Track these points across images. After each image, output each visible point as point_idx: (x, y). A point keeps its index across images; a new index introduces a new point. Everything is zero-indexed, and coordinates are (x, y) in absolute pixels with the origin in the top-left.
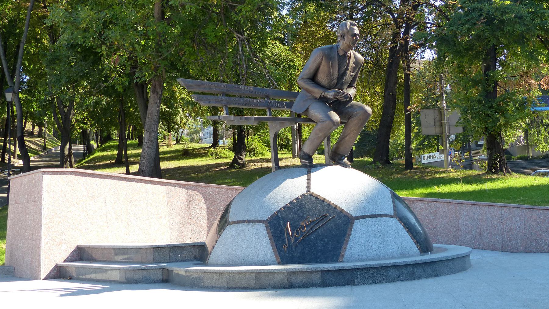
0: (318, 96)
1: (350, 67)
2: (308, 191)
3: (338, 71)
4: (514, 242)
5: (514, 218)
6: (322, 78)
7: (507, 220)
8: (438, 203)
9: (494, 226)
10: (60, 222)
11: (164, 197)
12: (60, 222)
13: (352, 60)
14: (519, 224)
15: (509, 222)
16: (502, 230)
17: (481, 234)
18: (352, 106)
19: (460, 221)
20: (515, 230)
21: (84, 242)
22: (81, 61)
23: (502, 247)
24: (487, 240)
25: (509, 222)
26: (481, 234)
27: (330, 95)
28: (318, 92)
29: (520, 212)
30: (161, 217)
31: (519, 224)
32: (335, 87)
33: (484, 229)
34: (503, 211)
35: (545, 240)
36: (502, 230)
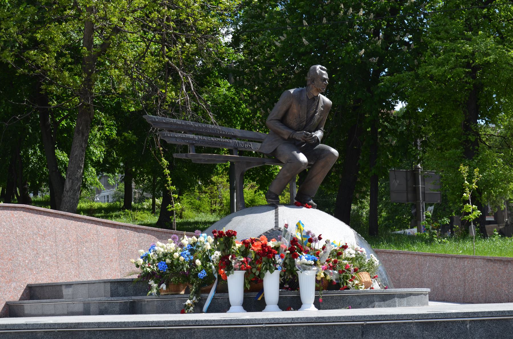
0: (286, 137)
1: (318, 110)
2: (276, 226)
3: (307, 113)
4: (475, 293)
5: (476, 270)
6: (292, 120)
7: (469, 271)
8: (402, 255)
9: (457, 277)
10: (10, 259)
11: (115, 240)
12: (10, 259)
13: (321, 104)
14: (481, 275)
15: (471, 273)
16: (464, 280)
17: (443, 286)
18: (319, 149)
19: (423, 273)
20: (477, 281)
21: (32, 281)
22: (435, 51)
23: (463, 299)
24: (449, 292)
25: (471, 273)
26: (443, 286)
27: (299, 135)
28: (286, 133)
29: (482, 263)
30: (111, 261)
31: (481, 275)
32: (303, 130)
33: (446, 281)
34: (466, 262)
35: (505, 291)
36: (464, 280)
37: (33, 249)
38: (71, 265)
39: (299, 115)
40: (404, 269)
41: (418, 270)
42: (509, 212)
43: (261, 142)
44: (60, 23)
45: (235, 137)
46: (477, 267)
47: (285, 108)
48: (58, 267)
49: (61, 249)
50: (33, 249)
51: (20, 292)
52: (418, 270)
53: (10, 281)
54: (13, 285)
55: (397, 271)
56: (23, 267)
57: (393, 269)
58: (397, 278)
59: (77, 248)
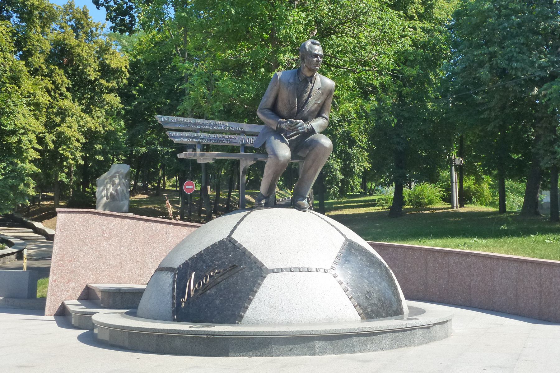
4: (553, 308)
5: (554, 280)
6: (282, 107)
7: (546, 281)
9: (532, 287)
10: (71, 261)
19: (495, 279)
24: (522, 304)
34: (543, 269)
37: (96, 251)
38: (135, 264)
39: (289, 101)
40: (475, 274)
41: (490, 276)
42: (179, 217)
43: (257, 135)
44: (336, 69)
45: (244, 133)
46: (555, 277)
47: (273, 95)
48: (121, 267)
49: (126, 250)
50: (96, 251)
51: (78, 291)
52: (490, 276)
53: (69, 281)
54: (72, 285)
55: (467, 276)
56: (83, 268)
57: (464, 273)
58: (467, 284)
59: (143, 249)
